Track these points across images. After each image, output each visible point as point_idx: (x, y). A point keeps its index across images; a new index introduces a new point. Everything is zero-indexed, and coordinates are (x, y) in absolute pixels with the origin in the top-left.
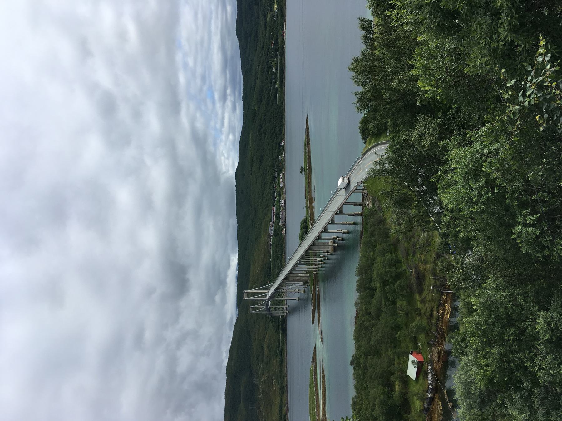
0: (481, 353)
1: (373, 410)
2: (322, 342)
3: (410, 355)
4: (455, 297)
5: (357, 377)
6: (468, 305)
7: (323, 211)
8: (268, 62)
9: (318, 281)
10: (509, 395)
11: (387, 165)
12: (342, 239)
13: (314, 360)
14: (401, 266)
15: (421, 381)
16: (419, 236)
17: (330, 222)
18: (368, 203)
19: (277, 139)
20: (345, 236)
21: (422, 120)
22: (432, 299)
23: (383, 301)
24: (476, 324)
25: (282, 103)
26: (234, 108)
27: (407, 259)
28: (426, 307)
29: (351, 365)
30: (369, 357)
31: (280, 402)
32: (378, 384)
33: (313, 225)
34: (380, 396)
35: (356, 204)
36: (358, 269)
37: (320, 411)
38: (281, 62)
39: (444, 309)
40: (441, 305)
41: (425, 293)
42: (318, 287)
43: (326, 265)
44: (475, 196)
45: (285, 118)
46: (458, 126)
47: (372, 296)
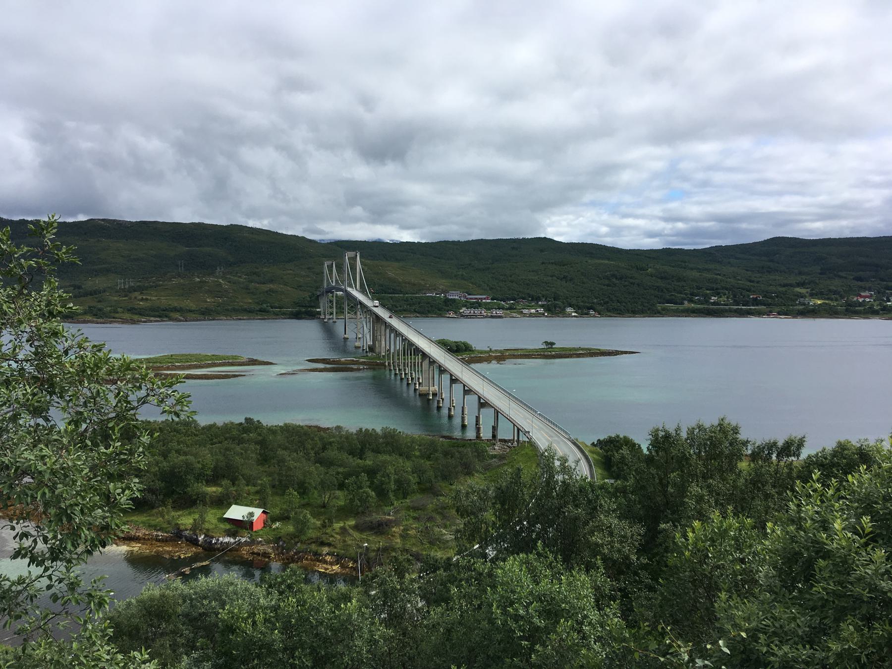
0: (272, 614)
1: (178, 452)
2: (280, 374)
3: (262, 510)
4: (351, 580)
5: (227, 428)
6: (347, 598)
7: (484, 376)
8: (727, 289)
9: (374, 369)
10: (210, 657)
11: (560, 478)
12: (440, 407)
13: (253, 362)
14: (397, 499)
15: (222, 526)
16: (445, 527)
17: (466, 388)
18: (496, 448)
19: (600, 304)
20: (445, 412)
21: (635, 531)
22: (347, 546)
23: (344, 470)
24: (318, 608)
25: (659, 312)
26: (651, 235)
27: (408, 508)
28: (336, 536)
29: (246, 419)
30: (258, 447)
31: (188, 308)
32: (217, 460)
33: (462, 362)
34: (199, 462)
35: (495, 429)
36: (394, 432)
37: (175, 370)
38: (726, 311)
39: (331, 564)
40: (339, 559)
41: (356, 535)
42: (364, 369)
43: (398, 382)
44: (517, 610)
45: (633, 317)
46: (625, 588)
47: (352, 453)
